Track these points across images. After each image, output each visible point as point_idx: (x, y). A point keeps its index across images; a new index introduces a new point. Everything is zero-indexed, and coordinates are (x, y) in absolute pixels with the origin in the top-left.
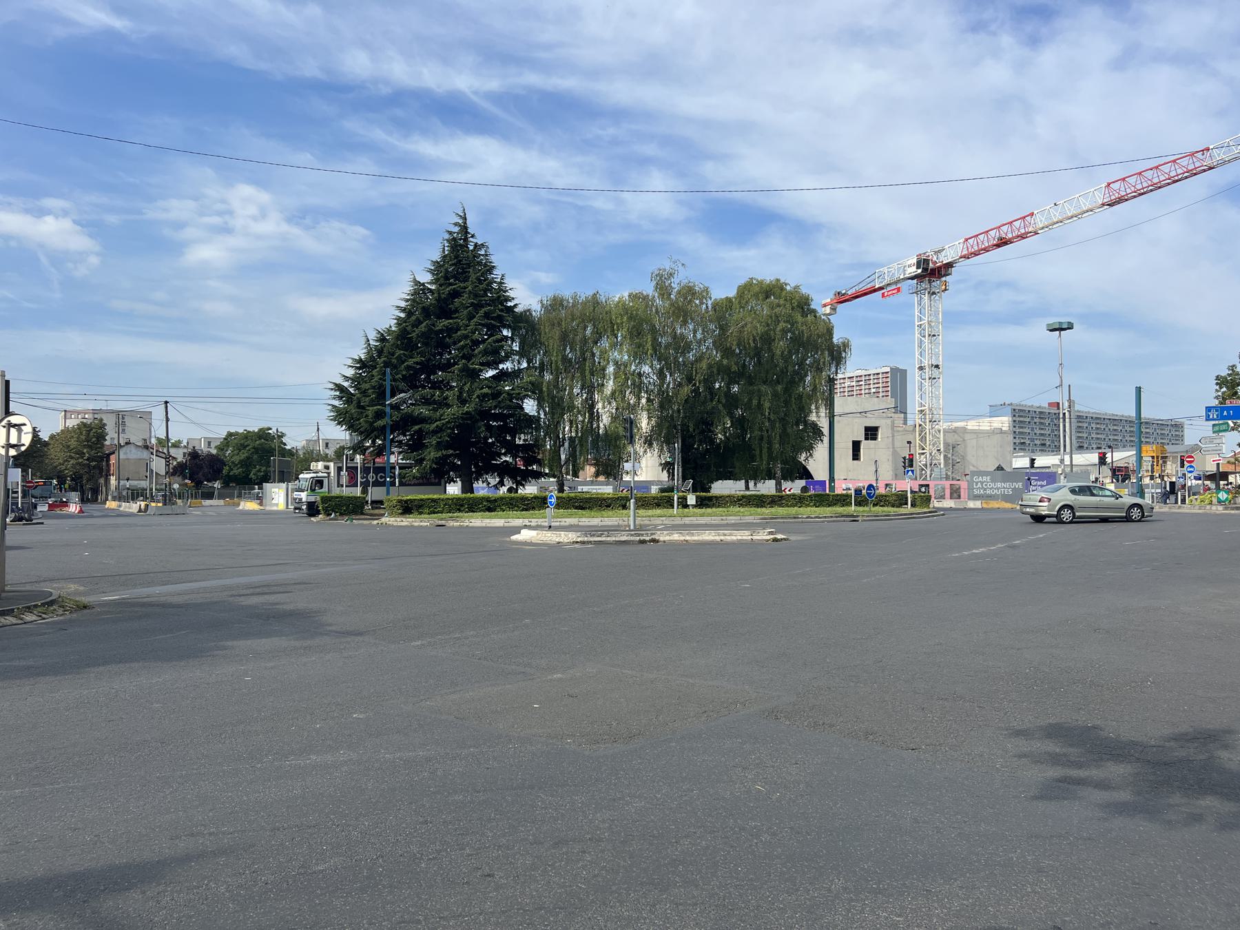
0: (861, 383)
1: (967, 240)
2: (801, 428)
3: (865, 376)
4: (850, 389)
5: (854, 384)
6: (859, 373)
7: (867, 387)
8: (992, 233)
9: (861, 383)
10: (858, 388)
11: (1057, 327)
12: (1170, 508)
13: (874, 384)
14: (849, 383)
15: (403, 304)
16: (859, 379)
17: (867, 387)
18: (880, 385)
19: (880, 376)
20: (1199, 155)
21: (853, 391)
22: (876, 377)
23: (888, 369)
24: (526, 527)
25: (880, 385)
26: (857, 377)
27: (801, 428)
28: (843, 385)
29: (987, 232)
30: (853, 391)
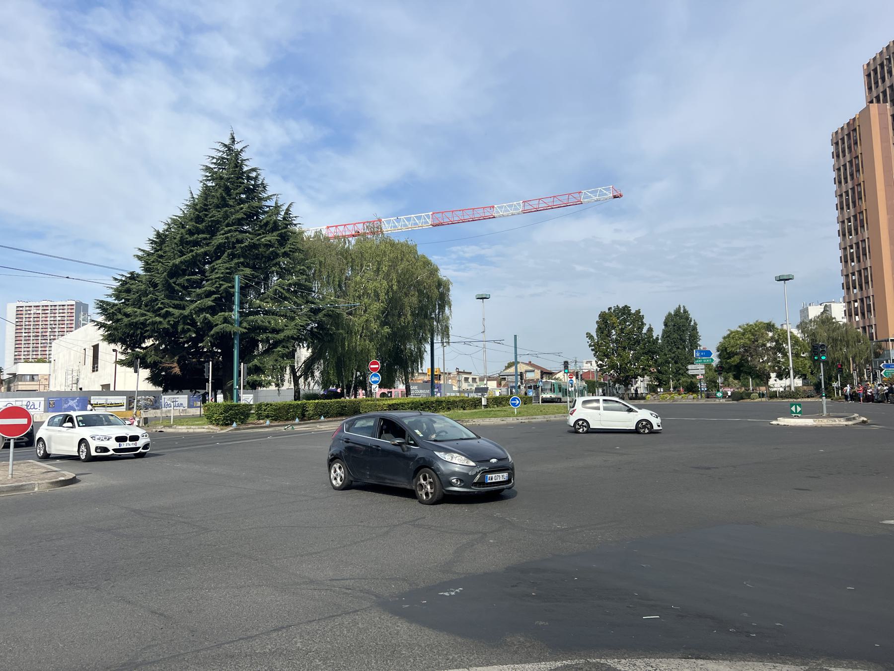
0: (47, 312)
1: (328, 227)
2: (185, 346)
3: (51, 306)
4: (36, 316)
5: (40, 312)
6: (45, 303)
7: (53, 315)
8: (350, 227)
9: (47, 312)
10: (44, 315)
11: (480, 297)
12: (726, 401)
13: (60, 313)
14: (35, 311)
15: (183, 207)
16: (45, 308)
17: (53, 315)
18: (66, 315)
19: (66, 307)
20: (488, 209)
21: (39, 317)
22: (61, 307)
23: (73, 303)
24: (357, 419)
25: (66, 315)
26: (43, 306)
27: (185, 346)
28: (29, 312)
29: (346, 225)
30: (39, 317)
